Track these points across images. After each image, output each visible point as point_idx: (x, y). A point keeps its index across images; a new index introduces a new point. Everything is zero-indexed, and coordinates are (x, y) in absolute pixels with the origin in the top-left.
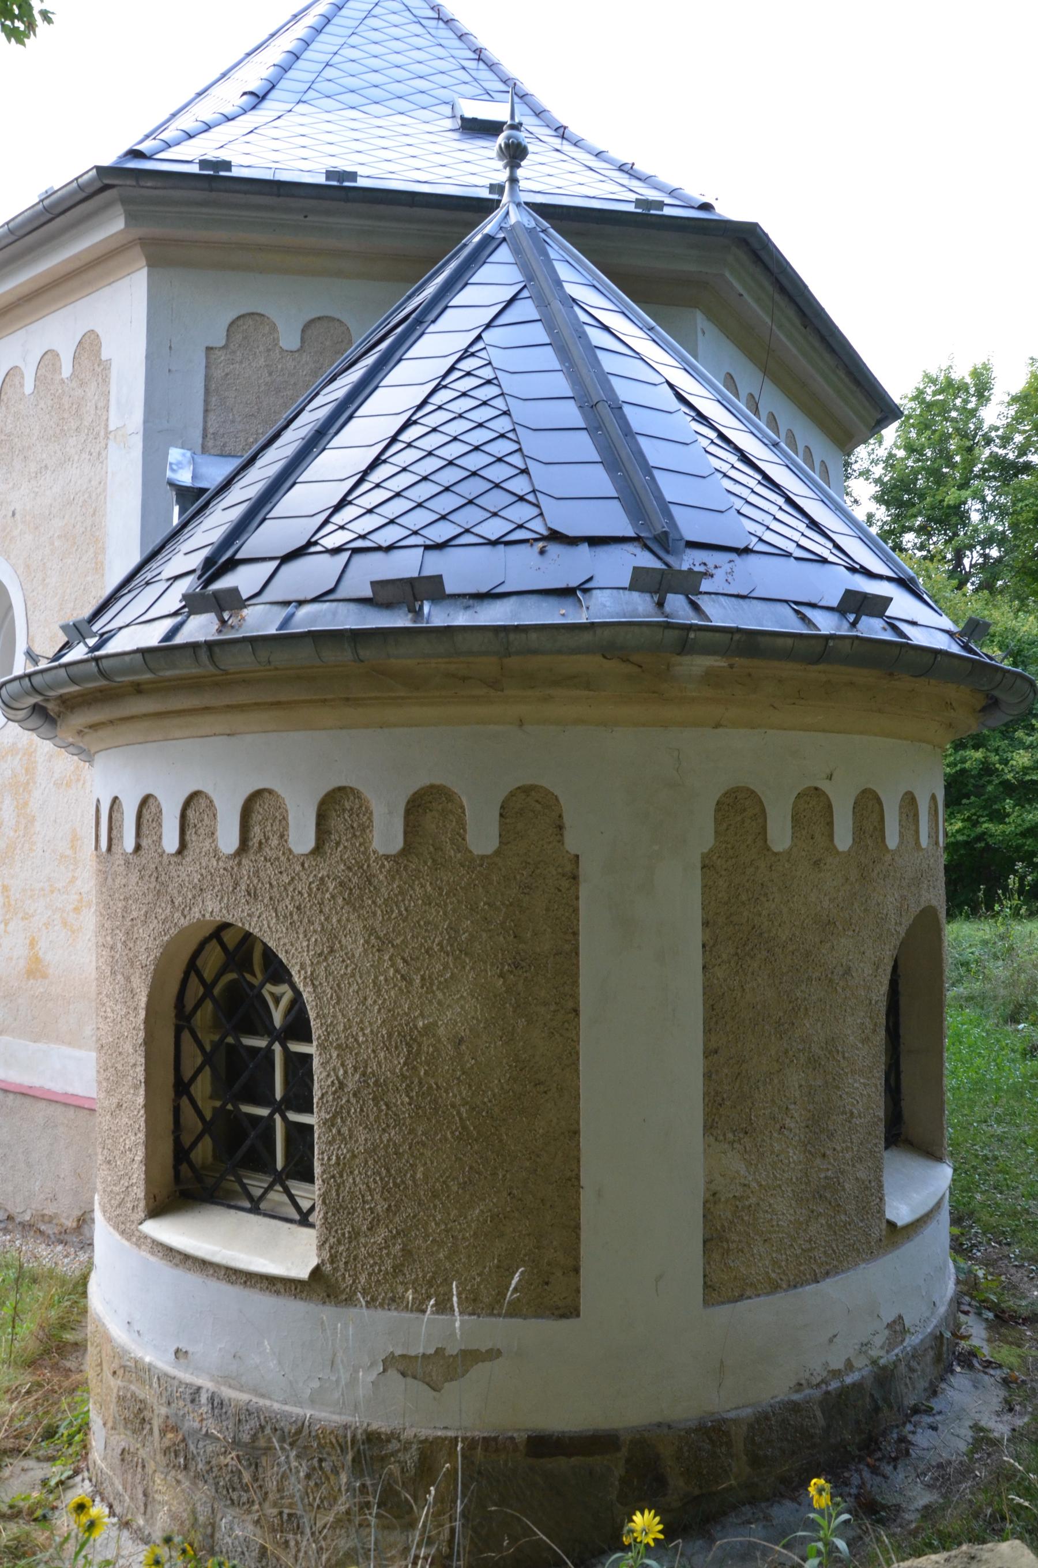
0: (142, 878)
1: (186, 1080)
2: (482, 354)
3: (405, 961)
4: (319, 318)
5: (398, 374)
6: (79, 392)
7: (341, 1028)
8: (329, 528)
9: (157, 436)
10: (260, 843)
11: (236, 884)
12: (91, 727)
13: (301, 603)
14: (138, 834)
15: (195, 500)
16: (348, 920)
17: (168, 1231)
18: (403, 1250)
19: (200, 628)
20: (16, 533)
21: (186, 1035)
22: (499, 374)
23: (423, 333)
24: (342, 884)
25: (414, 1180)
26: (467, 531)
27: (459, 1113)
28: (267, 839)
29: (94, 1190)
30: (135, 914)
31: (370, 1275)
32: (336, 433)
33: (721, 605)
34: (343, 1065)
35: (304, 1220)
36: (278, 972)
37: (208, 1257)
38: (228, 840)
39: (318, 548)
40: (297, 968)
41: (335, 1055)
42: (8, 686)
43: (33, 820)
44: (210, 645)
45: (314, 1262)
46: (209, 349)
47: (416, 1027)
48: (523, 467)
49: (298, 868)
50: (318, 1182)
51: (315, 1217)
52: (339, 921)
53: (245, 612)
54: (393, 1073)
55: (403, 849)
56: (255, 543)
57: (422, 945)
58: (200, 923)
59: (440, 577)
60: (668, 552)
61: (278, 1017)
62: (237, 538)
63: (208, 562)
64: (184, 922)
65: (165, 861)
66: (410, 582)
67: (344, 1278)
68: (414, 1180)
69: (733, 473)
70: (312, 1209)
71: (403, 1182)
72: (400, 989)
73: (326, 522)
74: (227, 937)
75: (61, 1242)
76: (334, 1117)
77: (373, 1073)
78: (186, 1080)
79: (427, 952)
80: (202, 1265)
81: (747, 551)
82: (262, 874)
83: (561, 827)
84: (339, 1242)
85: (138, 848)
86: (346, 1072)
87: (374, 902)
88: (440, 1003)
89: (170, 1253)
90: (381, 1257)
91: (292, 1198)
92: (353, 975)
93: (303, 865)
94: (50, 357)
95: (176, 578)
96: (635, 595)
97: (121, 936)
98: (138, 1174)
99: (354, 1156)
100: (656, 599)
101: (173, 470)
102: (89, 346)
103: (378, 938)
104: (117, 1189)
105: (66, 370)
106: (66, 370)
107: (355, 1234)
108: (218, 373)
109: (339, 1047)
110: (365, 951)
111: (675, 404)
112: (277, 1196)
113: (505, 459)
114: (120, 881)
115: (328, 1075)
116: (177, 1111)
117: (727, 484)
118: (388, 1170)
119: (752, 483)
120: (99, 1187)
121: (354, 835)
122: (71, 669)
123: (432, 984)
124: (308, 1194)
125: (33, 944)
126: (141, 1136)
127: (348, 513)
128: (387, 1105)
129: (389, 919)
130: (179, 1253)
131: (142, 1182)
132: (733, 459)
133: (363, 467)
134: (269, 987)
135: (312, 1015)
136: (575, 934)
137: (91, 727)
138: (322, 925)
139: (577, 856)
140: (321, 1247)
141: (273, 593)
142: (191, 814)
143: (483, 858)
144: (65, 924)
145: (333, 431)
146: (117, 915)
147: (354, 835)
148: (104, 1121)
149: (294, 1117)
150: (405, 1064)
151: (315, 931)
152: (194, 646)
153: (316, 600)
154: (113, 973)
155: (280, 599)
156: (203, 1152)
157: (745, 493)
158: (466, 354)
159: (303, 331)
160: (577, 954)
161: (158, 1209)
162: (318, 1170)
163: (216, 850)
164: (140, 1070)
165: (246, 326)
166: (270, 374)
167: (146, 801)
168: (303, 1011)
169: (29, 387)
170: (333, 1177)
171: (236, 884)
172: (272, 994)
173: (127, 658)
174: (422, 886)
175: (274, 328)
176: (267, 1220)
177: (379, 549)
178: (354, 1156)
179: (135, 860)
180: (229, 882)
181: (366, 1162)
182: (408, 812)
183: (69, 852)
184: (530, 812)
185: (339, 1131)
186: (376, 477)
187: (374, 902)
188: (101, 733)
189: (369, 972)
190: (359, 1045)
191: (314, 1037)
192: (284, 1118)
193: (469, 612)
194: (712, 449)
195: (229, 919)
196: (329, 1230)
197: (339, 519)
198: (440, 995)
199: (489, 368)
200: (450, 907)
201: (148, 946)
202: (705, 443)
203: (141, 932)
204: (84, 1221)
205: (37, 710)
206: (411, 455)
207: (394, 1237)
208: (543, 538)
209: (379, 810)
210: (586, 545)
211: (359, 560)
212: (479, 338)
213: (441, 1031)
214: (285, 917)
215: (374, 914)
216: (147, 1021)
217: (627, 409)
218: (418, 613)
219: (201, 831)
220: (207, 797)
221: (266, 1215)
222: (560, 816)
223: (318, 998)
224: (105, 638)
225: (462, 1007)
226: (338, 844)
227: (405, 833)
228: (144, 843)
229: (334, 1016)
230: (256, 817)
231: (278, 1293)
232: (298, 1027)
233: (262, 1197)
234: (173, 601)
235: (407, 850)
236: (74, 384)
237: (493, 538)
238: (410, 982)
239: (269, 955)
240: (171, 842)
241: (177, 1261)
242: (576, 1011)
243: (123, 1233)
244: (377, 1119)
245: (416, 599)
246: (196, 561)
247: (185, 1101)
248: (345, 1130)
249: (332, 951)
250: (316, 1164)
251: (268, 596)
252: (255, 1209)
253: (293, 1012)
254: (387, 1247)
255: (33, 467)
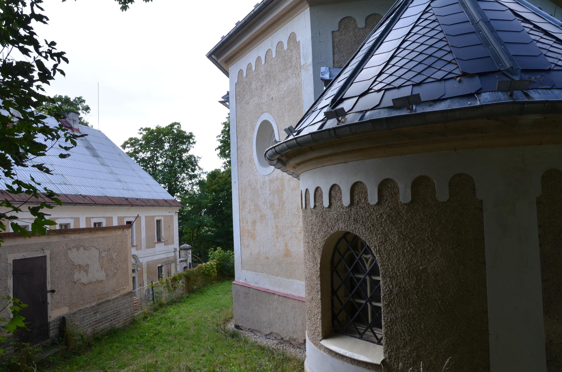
0: (317, 217)
1: (335, 290)
2: (431, 11)
3: (414, 244)
4: (371, 15)
5: (399, 24)
6: (290, 54)
7: (390, 270)
8: (377, 83)
9: (316, 65)
10: (358, 202)
11: (350, 217)
12: (297, 165)
13: (366, 111)
14: (315, 202)
15: (329, 83)
16: (391, 229)
17: (327, 344)
18: (416, 355)
19: (332, 123)
20: (273, 105)
21: (335, 273)
22: (438, 17)
23: (407, 8)
24: (388, 215)
25: (420, 329)
26: (429, 77)
27: (437, 303)
28: (360, 200)
29: (306, 329)
30: (315, 230)
31: (404, 364)
32: (377, 49)
33: (539, 93)
34: (391, 284)
35: (379, 342)
36: (368, 251)
37: (344, 354)
38: (346, 201)
39: (373, 91)
40: (373, 247)
41: (388, 280)
42: (268, 152)
43: (284, 203)
44: (334, 129)
45: (383, 358)
46: (333, 32)
47: (419, 269)
48: (449, 50)
49: (372, 210)
50: (383, 328)
51: (383, 342)
52: (388, 229)
53: (347, 116)
54: (411, 287)
55: (411, 201)
56: (349, 92)
57: (420, 238)
58: (338, 232)
59: (419, 94)
60: (513, 75)
61: (368, 267)
62: (343, 91)
63: (333, 101)
64: (332, 232)
65: (325, 210)
66: (407, 98)
67: (394, 365)
68: (420, 329)
69: (542, 40)
70: (382, 338)
71: (416, 329)
72: (413, 255)
73: (375, 81)
74: (349, 238)
75: (299, 348)
76: (389, 304)
77: (403, 287)
78: (335, 290)
79: (422, 240)
80: (342, 357)
81: (550, 70)
82: (359, 213)
83: (474, 189)
84: (392, 351)
85: (315, 206)
86: (393, 286)
87: (401, 222)
88: (428, 260)
89: (330, 352)
90: (408, 357)
91: (374, 334)
92: (394, 250)
93: (374, 209)
94: (280, 44)
95: (322, 108)
96: (500, 93)
97: (311, 238)
98: (319, 323)
99: (397, 319)
100: (509, 94)
101: (322, 75)
102: (292, 37)
103: (403, 235)
104: (312, 328)
105: (286, 47)
106: (286, 47)
107: (398, 348)
108: (337, 40)
109: (390, 277)
110: (399, 240)
111: (513, 16)
112: (369, 333)
113: (443, 48)
114: (310, 218)
115: (386, 288)
116: (332, 301)
117: (539, 45)
118: (410, 324)
119: (551, 43)
120: (307, 328)
121: (392, 197)
122: (287, 143)
123: (425, 253)
124: (381, 333)
125: (286, 245)
126: (320, 309)
127: (383, 76)
128: (409, 299)
129: (407, 228)
130: (334, 352)
131: (320, 326)
132: (541, 34)
133: (388, 59)
134: (364, 255)
135: (379, 265)
136: (483, 232)
137: (297, 165)
138: (382, 231)
139: (482, 201)
140: (385, 353)
141: (356, 109)
142: (333, 193)
143: (443, 203)
144: (296, 238)
145: (375, 48)
146: (309, 231)
147: (392, 197)
148: (308, 304)
149: (375, 304)
150: (415, 283)
151: (379, 233)
152: (329, 130)
153: (373, 109)
154: (309, 252)
155: (359, 110)
156: (342, 316)
157: (548, 47)
158: (425, 12)
159: (366, 20)
160: (484, 240)
161: (327, 336)
162: (383, 323)
163: (342, 205)
164: (319, 286)
165: (345, 22)
166: (355, 37)
167: (317, 189)
168: (376, 265)
169: (274, 56)
170: (389, 326)
171: (350, 217)
172: (365, 258)
173: (306, 137)
174: (420, 215)
175: (355, 21)
176: (365, 342)
177: (395, 88)
178: (397, 319)
179: (314, 211)
180: (347, 217)
181: (401, 321)
182: (412, 187)
183: (297, 213)
184: (461, 184)
185: (391, 309)
186: (392, 62)
187: (401, 222)
188: (301, 166)
189: (400, 249)
190: (398, 276)
191: (381, 273)
192: (371, 304)
193: (431, 107)
194: (532, 32)
195: (348, 230)
196: (388, 346)
197: (379, 79)
198: (428, 257)
199: (434, 16)
200: (431, 222)
201: (320, 241)
202: (528, 30)
203: (318, 236)
204: (305, 341)
205: (279, 160)
206: (406, 52)
207: (413, 350)
208: (459, 76)
209: (401, 186)
210: (478, 77)
211: (388, 93)
212: (429, 6)
213: (429, 271)
214: (368, 228)
215: (402, 226)
216: (320, 268)
217: (492, 22)
218: (411, 109)
219: (337, 199)
220: (338, 186)
221: (365, 340)
222: (474, 185)
223: (381, 258)
224: (299, 132)
225: (437, 262)
226: (386, 200)
227: (412, 195)
228: (317, 204)
229: (388, 265)
230: (356, 192)
231: (369, 369)
232: (375, 271)
233: (364, 333)
234: (322, 116)
235: (413, 202)
236: (289, 52)
237: (439, 78)
238: (416, 252)
239: (363, 244)
240: (326, 204)
241: (333, 355)
242: (484, 263)
243: (315, 344)
244: (405, 304)
245: (410, 104)
246: (329, 101)
247: (335, 297)
248: (393, 308)
249: (386, 241)
250: (383, 321)
251: (355, 110)
252: (361, 338)
253: (373, 264)
254: (410, 354)
255: (277, 82)
